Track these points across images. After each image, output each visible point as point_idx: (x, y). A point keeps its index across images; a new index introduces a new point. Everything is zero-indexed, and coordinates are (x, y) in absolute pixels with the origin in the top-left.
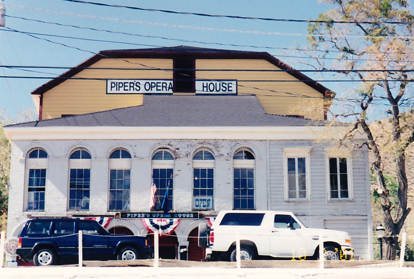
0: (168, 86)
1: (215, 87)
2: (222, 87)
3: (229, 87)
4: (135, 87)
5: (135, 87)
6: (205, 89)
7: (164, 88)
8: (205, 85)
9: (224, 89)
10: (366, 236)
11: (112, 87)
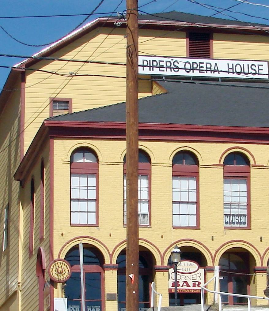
2: (250, 71)
3: (259, 70)
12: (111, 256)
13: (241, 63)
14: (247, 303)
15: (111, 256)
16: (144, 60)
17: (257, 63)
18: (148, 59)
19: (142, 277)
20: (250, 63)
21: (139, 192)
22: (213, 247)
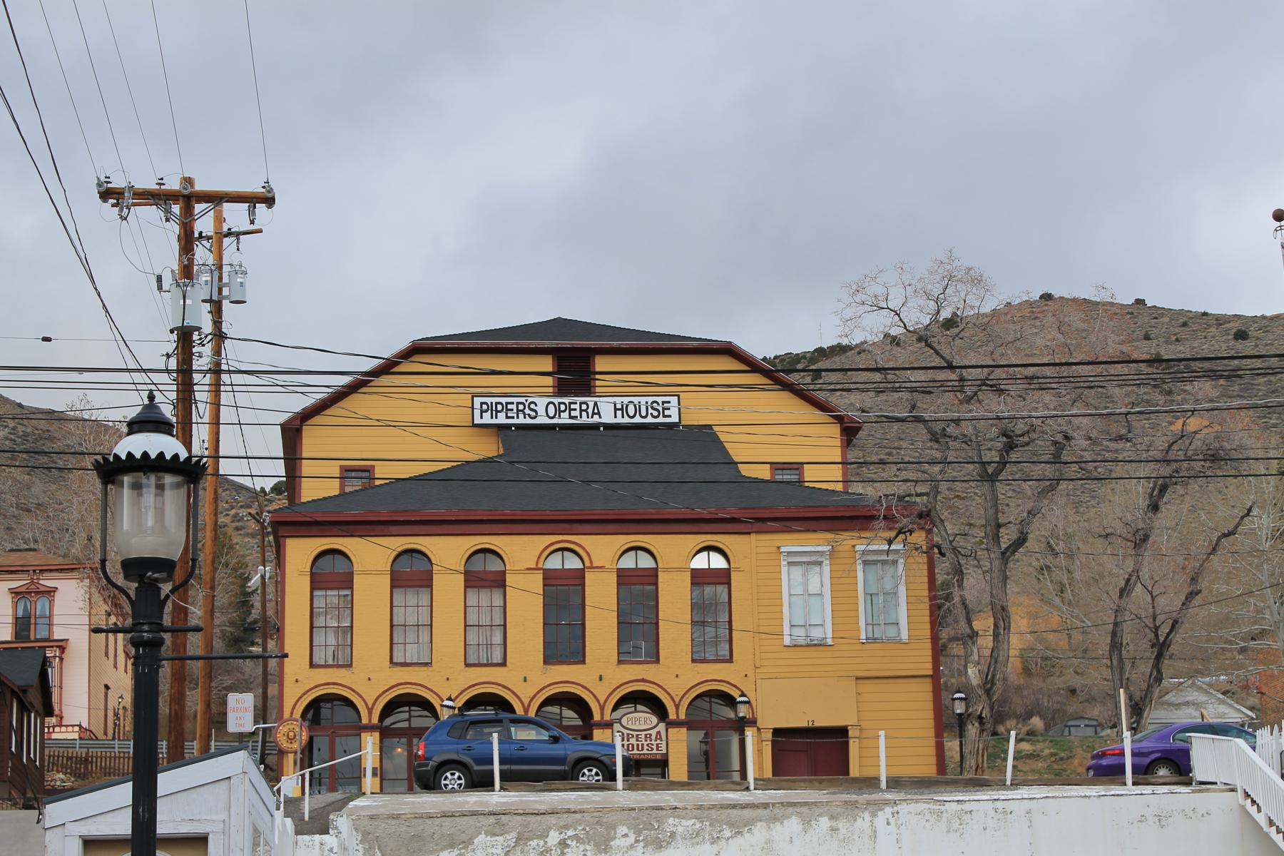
0: (590, 411)
1: (637, 409)
2: (650, 411)
3: (664, 409)
4: (527, 411)
5: (527, 411)
6: (619, 413)
7: (584, 414)
8: (619, 406)
9: (655, 413)
10: (506, 767)
11: (482, 412)
12: (370, 711)
13: (636, 400)
14: (506, 767)
15: (370, 711)
16: (482, 404)
17: (660, 399)
18: (488, 400)
19: (1190, 771)
20: (650, 399)
21: (32, 627)
22: (526, 692)
